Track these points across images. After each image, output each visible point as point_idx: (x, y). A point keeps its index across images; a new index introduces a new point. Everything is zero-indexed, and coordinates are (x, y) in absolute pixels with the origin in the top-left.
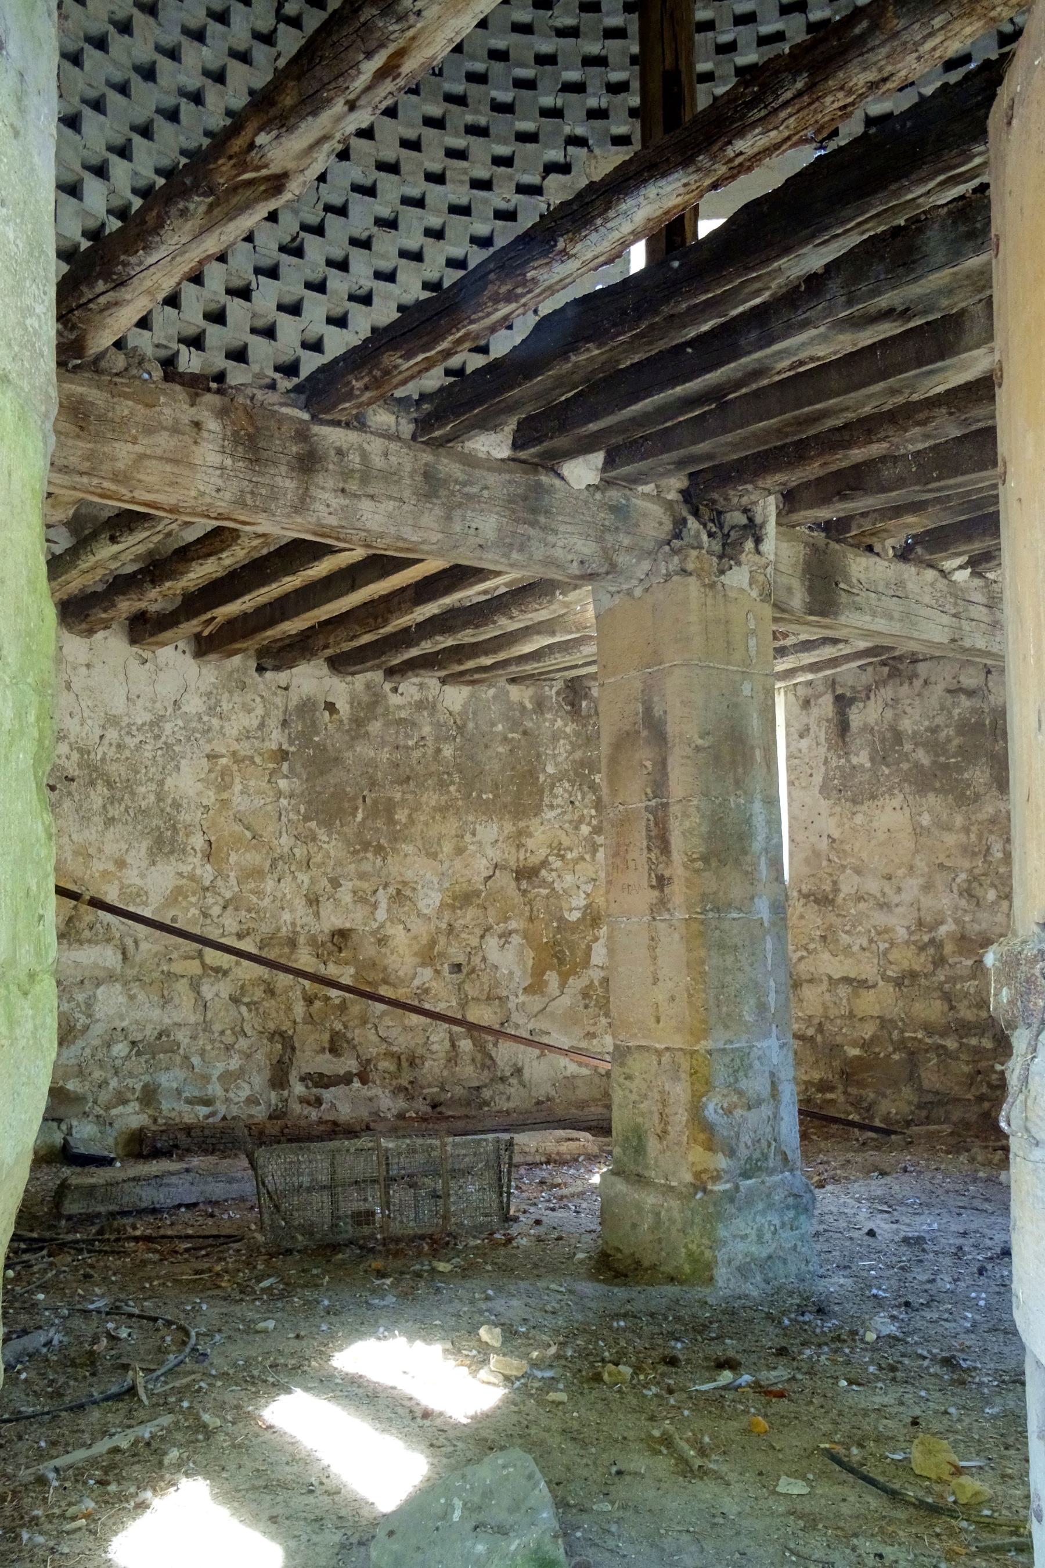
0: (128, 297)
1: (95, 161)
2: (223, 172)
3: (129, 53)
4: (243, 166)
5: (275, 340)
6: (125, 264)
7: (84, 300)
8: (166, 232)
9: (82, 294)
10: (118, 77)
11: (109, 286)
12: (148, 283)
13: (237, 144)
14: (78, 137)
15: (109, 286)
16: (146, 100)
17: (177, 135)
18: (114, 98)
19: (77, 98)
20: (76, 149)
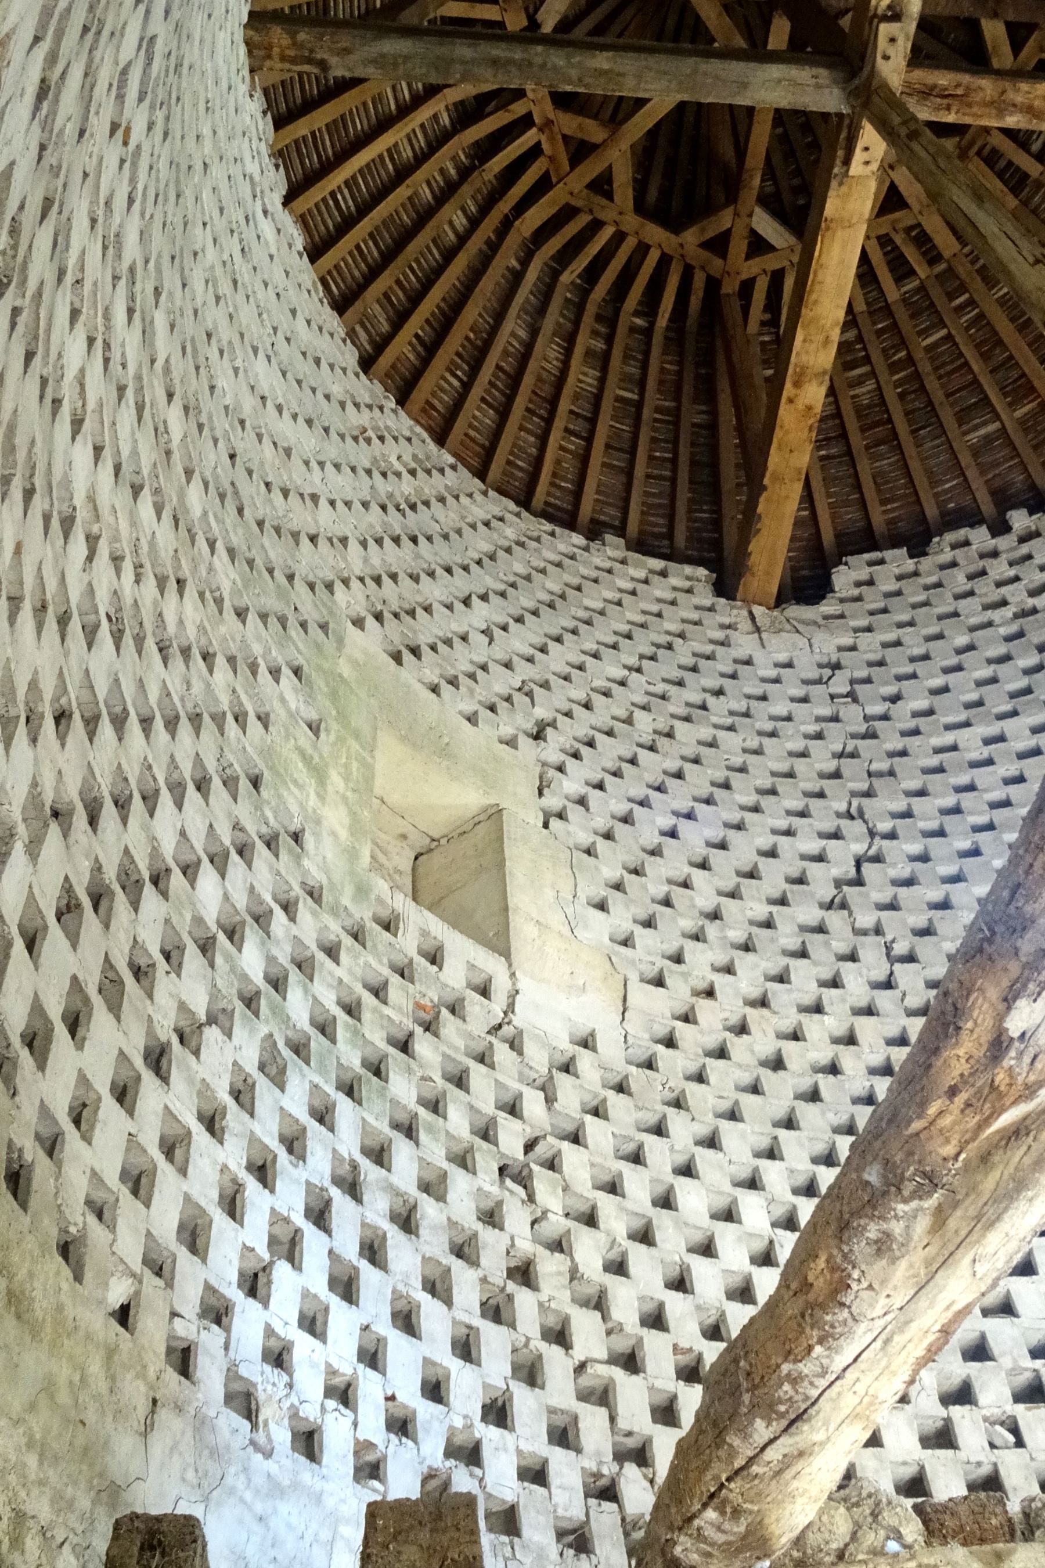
0: (819, 1436)
1: (745, 1174)
2: (946, 1126)
3: (752, 1052)
4: (994, 1098)
5: (1017, 1316)
6: (795, 1380)
7: (738, 1463)
8: (857, 1296)
9: (733, 1453)
10: (747, 1079)
11: (777, 1426)
12: (849, 1402)
13: (961, 1055)
14: (721, 1155)
15: (777, 1426)
16: (782, 1090)
17: (823, 1114)
18: (749, 1101)
19: (711, 1115)
20: (721, 1168)
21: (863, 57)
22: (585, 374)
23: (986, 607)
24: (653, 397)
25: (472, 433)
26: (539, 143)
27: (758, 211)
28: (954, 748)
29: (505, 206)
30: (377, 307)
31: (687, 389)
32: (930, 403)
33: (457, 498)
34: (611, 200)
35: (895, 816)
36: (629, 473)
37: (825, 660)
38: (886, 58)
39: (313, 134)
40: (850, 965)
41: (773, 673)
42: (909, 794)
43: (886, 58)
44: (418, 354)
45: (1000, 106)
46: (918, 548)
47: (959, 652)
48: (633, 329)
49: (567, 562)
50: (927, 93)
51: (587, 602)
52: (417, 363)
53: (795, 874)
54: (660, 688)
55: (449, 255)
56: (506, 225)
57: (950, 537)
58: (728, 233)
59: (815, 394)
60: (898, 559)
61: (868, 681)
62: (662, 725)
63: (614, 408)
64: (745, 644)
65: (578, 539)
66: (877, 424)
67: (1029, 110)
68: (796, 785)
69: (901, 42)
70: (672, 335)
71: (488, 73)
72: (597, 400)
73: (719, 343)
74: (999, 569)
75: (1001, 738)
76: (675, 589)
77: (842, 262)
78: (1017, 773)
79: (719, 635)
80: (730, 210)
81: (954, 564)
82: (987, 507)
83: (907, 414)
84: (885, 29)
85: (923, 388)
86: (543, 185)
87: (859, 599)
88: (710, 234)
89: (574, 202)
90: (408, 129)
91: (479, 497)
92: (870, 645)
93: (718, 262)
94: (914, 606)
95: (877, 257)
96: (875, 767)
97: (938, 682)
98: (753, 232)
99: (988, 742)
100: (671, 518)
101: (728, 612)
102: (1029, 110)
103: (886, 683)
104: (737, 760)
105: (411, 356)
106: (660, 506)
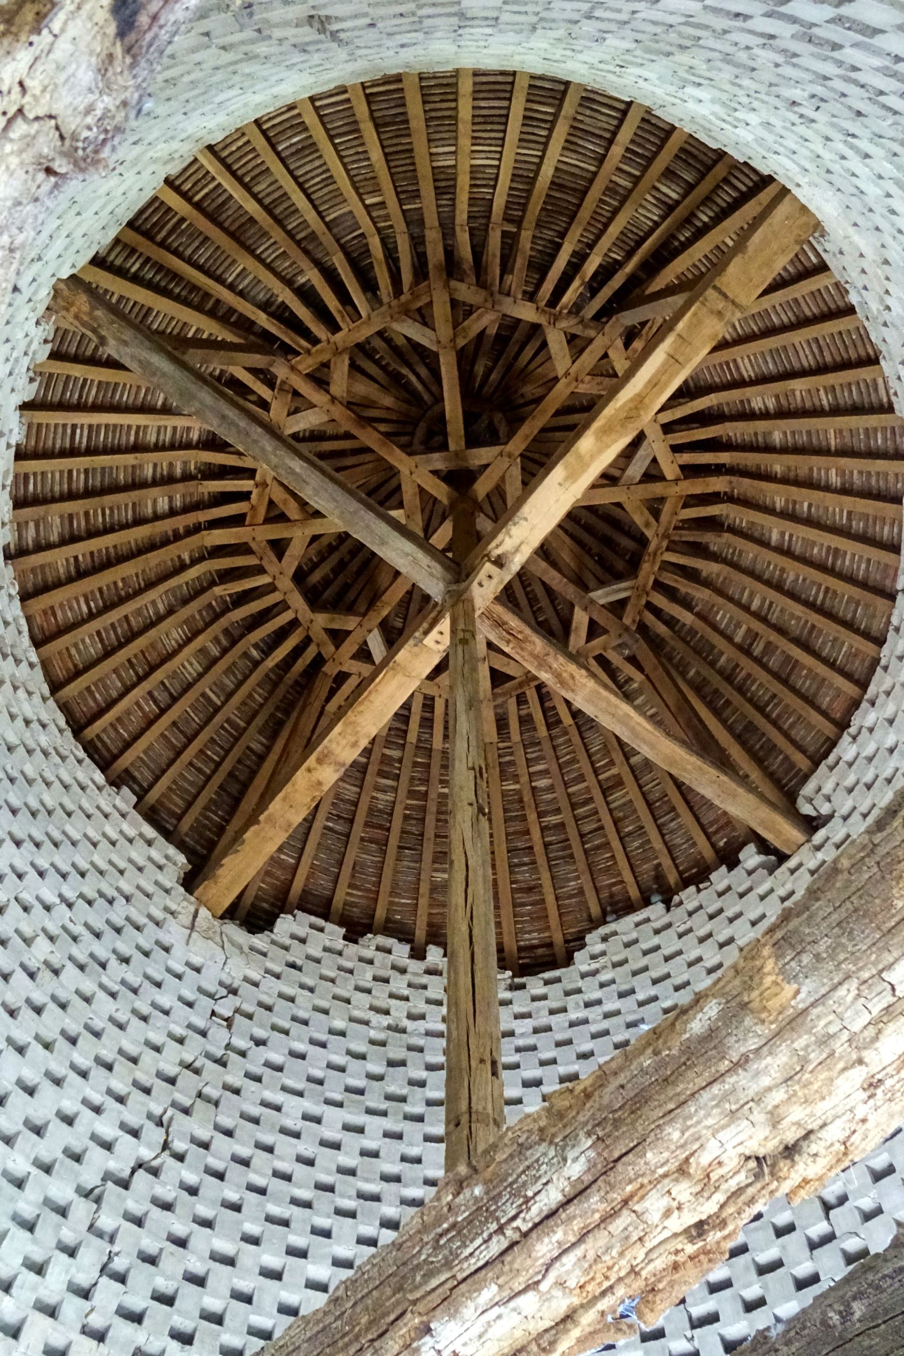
21: (467, 576)
22: (191, 664)
23: (372, 1008)
24: (230, 710)
25: (73, 651)
26: (250, 493)
27: (376, 632)
28: (278, 1109)
29: (203, 516)
30: (58, 521)
31: (259, 720)
32: (422, 835)
33: (15, 688)
34: (280, 560)
35: (194, 1141)
36: (179, 754)
37: (228, 981)
38: (481, 585)
39: (85, 380)
40: (64, 1257)
41: (179, 968)
42: (217, 1128)
43: (481, 585)
44: (69, 571)
45: (542, 663)
46: (352, 937)
47: (332, 1032)
48: (246, 655)
49: (76, 788)
50: (499, 624)
51: (69, 829)
52: (63, 577)
53: (77, 1148)
54: (78, 929)
55: (139, 521)
56: (196, 529)
57: (381, 940)
58: (348, 633)
59: (329, 776)
60: (334, 934)
61: (250, 1017)
62: (56, 960)
63: (197, 700)
64: (174, 933)
65: (100, 778)
66: (381, 827)
67: (558, 676)
68: (131, 1071)
69: (495, 581)
70: (272, 676)
71: (215, 422)
72: (188, 687)
73: (301, 703)
74: (399, 984)
75: (318, 1120)
76: (150, 859)
77: (392, 697)
78: (312, 1156)
79: (159, 914)
80: (358, 619)
81: (371, 962)
82: (420, 934)
83: (403, 832)
84: (488, 567)
85: (423, 820)
86: (238, 520)
87: (286, 948)
88: (335, 626)
89: (254, 546)
90: (162, 423)
91: (37, 699)
92: (270, 989)
93: (332, 648)
94: (323, 978)
95: (417, 708)
96: (207, 1090)
97: (300, 1047)
98: (365, 643)
99: (306, 1117)
100: (190, 804)
101: (180, 901)
102: (558, 676)
103: (261, 1026)
104: (98, 1024)
105: (61, 570)
106: (186, 791)
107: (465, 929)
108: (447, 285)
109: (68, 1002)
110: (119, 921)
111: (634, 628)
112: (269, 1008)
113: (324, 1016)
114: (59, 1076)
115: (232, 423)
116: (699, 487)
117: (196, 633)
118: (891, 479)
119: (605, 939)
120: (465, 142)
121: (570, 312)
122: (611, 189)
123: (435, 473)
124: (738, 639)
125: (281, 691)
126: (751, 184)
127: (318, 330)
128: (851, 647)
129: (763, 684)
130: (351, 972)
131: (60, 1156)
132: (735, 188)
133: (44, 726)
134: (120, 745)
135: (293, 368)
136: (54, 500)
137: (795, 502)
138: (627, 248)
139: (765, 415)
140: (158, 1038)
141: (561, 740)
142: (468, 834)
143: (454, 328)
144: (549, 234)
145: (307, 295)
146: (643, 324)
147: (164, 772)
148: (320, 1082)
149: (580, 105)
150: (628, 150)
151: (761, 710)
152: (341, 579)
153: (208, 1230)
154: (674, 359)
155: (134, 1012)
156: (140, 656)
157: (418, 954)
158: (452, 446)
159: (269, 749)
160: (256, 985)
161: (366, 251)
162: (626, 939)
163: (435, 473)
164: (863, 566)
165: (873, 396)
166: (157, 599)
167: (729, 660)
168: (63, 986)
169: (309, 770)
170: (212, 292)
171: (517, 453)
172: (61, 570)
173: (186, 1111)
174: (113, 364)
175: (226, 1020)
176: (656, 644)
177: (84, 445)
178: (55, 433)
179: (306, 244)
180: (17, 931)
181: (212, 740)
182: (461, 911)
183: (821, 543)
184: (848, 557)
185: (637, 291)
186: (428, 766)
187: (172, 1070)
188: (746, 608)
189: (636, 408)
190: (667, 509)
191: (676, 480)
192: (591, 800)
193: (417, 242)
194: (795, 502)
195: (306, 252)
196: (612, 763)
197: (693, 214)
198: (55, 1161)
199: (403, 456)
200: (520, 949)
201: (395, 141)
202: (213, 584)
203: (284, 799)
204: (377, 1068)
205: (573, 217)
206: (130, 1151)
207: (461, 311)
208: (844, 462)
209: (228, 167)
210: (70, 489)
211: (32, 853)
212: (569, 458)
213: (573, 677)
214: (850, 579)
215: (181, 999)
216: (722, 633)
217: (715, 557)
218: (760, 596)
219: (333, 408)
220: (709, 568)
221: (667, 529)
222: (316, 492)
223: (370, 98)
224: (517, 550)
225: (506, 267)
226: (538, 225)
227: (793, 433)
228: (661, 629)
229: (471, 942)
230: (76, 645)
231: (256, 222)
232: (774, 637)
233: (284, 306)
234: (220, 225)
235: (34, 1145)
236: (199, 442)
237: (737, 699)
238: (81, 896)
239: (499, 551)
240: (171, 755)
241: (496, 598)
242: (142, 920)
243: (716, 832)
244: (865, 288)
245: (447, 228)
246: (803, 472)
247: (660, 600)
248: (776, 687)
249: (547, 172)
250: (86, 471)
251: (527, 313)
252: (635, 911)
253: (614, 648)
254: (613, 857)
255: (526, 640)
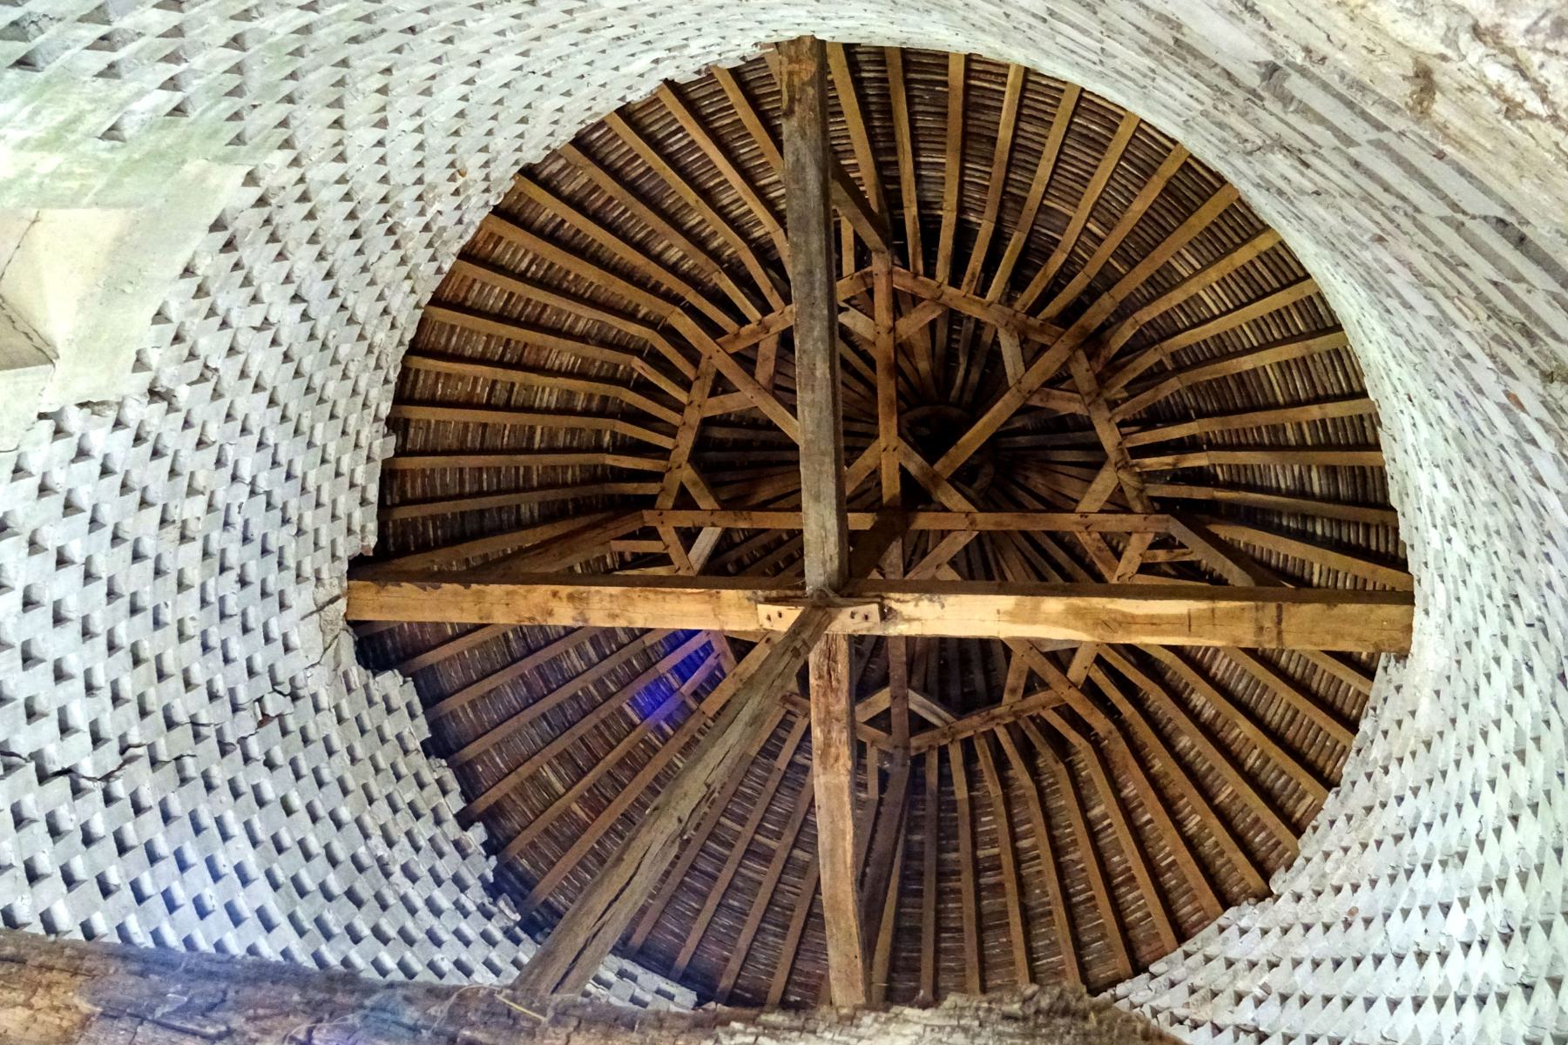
21: (850, 596)
22: (551, 394)
23: (383, 828)
24: (538, 463)
25: (477, 287)
26: (749, 322)
28: (225, 837)
29: (692, 297)
31: (551, 495)
33: (408, 277)
36: (462, 451)
37: (299, 683)
39: (731, 107)
41: (275, 633)
48: (599, 433)
49: (359, 400)
50: (830, 656)
51: (319, 427)
52: (537, 223)
54: (237, 519)
55: (641, 247)
56: (675, 300)
57: (449, 776)
58: (696, 507)
59: (564, 616)
60: (417, 731)
61: (285, 732)
62: (194, 528)
64: (302, 599)
66: (546, 681)
67: (827, 744)
69: (866, 624)
70: (599, 471)
73: (599, 516)
74: (424, 830)
76: (350, 516)
79: (308, 570)
82: (482, 803)
84: (874, 609)
85: (585, 714)
86: (715, 331)
89: (703, 362)
90: (745, 198)
91: (413, 299)
94: (372, 759)
95: (693, 645)
96: (188, 761)
97: (296, 802)
98: (700, 529)
99: (239, 869)
100: (424, 500)
101: (334, 576)
102: (827, 744)
103: (285, 752)
104: (168, 616)
105: (542, 218)
107: (581, 941)
108: (1073, 350)
109: (165, 573)
110: (273, 545)
111: (913, 753)
112: (306, 741)
113: (340, 794)
114: (92, 628)
115: (812, 285)
116: (1084, 708)
117: (582, 375)
118: (1235, 876)
119: (622, 974)
120: (1213, 275)
121: (1140, 474)
122: (1276, 429)
123: (903, 470)
124: (981, 853)
125: (595, 489)
126: (1382, 550)
127: (942, 269)
128: (1062, 963)
129: (963, 910)
130: (398, 777)
131: (21, 700)
132: (1367, 539)
133: (393, 326)
134: (427, 395)
135: (890, 273)
136: (600, 163)
137: (1141, 804)
138: (1236, 478)
139: (1194, 715)
140: (198, 676)
141: (758, 771)
142: (656, 848)
143: (1044, 385)
144: (1190, 400)
145: (965, 234)
146: (1182, 546)
147: (434, 453)
148: (280, 850)
149: (1328, 352)
150: (1323, 421)
151: (939, 929)
152: (736, 454)
153: (64, 888)
154: (1188, 623)
155: (204, 634)
156: (521, 346)
157: (465, 820)
158: (938, 466)
159: (533, 524)
160: (317, 709)
161: (1046, 256)
162: (638, 993)
163: (903, 470)
164: (1139, 914)
165: (1291, 802)
166: (586, 318)
167: (957, 862)
168: (176, 556)
169: (555, 594)
170: (900, 150)
171: (980, 527)
172: (542, 218)
173: (154, 763)
174: (775, 134)
175: (263, 714)
176: (916, 783)
177: (672, 149)
178: (662, 118)
179: (1011, 201)
180: (192, 474)
181: (498, 470)
182: (591, 920)
183: (1127, 857)
184: (1135, 894)
185: (1206, 517)
186: (637, 675)
187: (180, 715)
188: (1014, 838)
189: (1120, 624)
190: (1042, 696)
191: (1073, 685)
192: (730, 846)
193: (1092, 294)
194: (1141, 804)
195: (1002, 206)
196: (778, 836)
197: (1314, 519)
198: (13, 700)
199: (894, 431)
200: (546, 904)
201: (1163, 212)
202: (638, 352)
203: (508, 593)
204: (336, 887)
205: (1223, 412)
206: (76, 752)
207: (1059, 380)
208: (1214, 823)
209: (1024, 89)
210: (621, 168)
211: (272, 422)
212: (1028, 601)
213: (837, 760)
214: (1118, 911)
215: (249, 660)
216: (974, 835)
217: (1034, 772)
218: (1035, 841)
219: (884, 335)
220: (1018, 770)
221: (1023, 711)
222: (813, 404)
223: (1186, 167)
224: (909, 620)
225: (1136, 387)
226: (1190, 388)
227: (1199, 754)
228: (932, 778)
229: (575, 960)
230: (484, 285)
231: (994, 145)
232: (1011, 887)
233: (938, 220)
234: (965, 117)
235: (10, 670)
236: (755, 240)
237: (929, 899)
238: (269, 494)
239: (894, 605)
240: (455, 446)
241: (850, 636)
242: (290, 561)
243: (800, 985)
244: (1385, 733)
245: (1124, 311)
246: (1173, 791)
247: (956, 754)
248: (970, 927)
249: (1247, 363)
250: (649, 169)
251: (1108, 436)
252: (667, 977)
253: (881, 752)
254: (698, 912)
255: (835, 691)
